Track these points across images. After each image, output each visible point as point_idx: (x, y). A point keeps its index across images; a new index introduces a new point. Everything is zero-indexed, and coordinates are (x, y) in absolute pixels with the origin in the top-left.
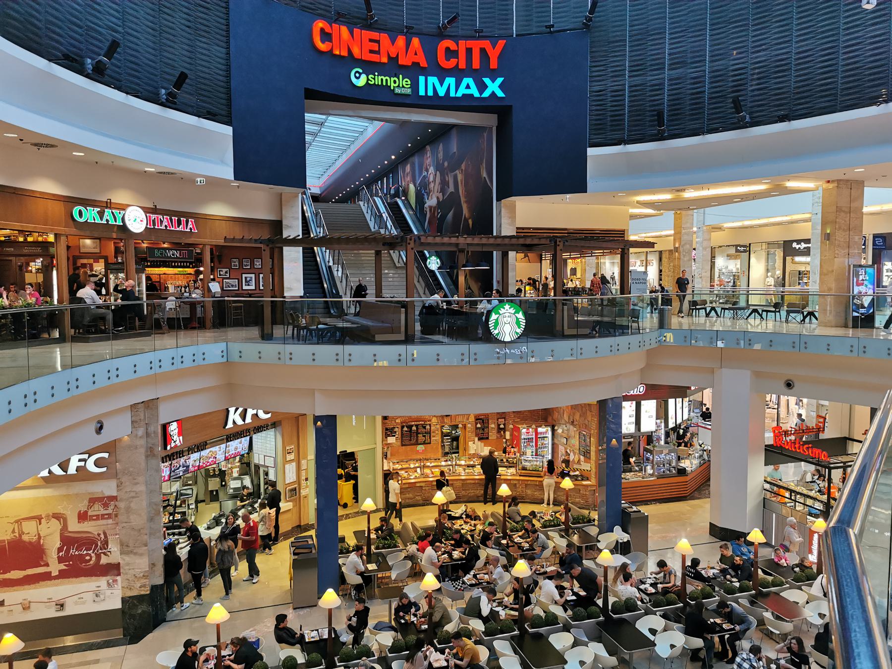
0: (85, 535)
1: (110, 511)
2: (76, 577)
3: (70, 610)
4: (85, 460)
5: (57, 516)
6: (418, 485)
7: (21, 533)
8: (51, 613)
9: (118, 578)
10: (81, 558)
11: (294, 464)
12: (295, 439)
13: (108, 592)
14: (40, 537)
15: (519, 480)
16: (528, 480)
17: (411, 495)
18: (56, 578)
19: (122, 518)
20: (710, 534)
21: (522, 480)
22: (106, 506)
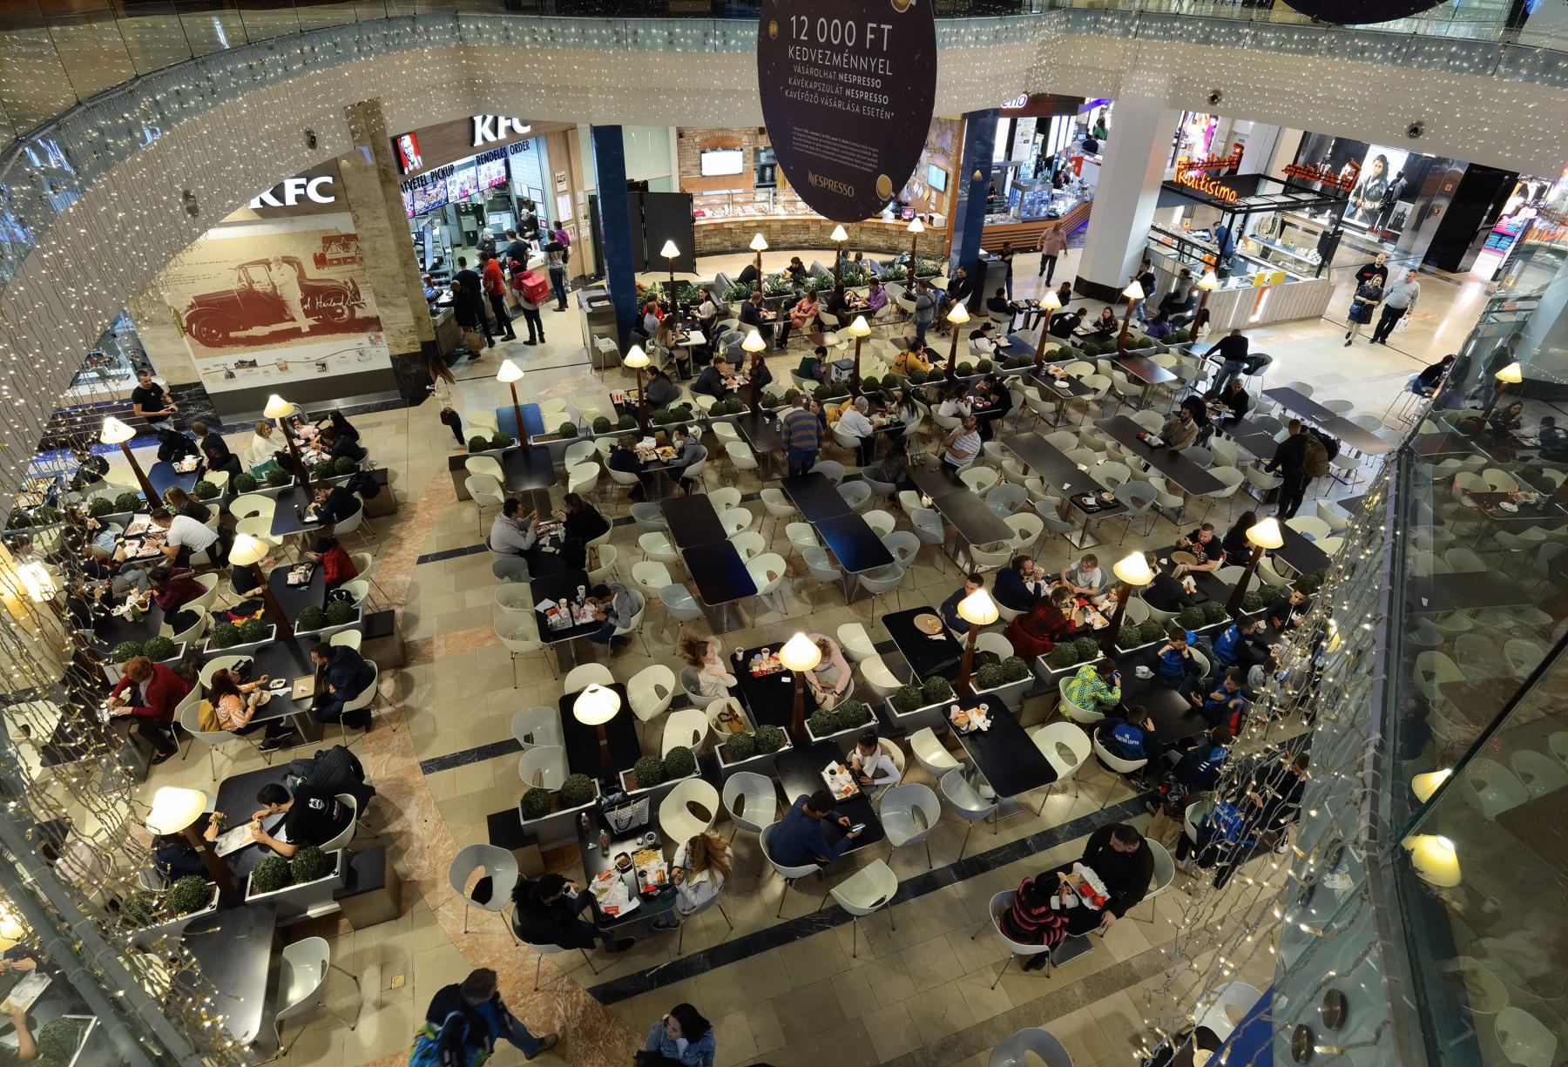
0: (328, 284)
1: (352, 254)
3: (335, 370)
5: (289, 261)
6: (726, 226)
7: (251, 282)
8: (313, 374)
9: (381, 334)
10: (332, 311)
11: (568, 197)
13: (373, 350)
14: (274, 287)
17: (717, 240)
22: (345, 247)
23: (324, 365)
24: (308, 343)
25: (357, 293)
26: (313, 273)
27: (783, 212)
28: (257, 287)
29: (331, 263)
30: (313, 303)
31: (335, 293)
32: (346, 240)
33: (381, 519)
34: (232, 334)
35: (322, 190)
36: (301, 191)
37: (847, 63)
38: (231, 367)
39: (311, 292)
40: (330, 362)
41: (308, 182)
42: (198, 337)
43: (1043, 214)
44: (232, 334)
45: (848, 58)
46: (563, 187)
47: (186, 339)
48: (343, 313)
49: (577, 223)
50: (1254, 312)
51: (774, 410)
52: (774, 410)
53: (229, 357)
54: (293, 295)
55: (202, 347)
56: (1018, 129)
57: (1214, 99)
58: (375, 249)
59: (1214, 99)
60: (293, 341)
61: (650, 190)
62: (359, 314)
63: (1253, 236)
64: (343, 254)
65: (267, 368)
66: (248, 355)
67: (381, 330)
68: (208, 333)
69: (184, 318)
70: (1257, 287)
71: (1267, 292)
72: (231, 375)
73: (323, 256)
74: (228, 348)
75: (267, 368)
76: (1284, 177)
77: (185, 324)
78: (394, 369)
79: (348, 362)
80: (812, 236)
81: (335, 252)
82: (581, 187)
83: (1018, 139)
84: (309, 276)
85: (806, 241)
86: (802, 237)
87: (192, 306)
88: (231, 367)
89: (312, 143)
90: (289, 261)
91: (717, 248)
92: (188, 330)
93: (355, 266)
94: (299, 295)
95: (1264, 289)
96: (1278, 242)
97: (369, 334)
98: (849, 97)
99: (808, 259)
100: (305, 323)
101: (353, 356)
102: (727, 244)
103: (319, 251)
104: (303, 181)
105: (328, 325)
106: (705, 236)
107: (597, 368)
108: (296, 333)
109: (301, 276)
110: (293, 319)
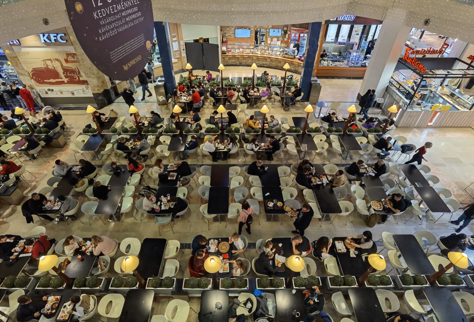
0: (70, 68)
1: (76, 59)
2: (71, 84)
3: (76, 95)
4: (56, 37)
5: (57, 60)
6: (237, 56)
7: (47, 66)
8: (70, 95)
9: (89, 86)
10: (73, 77)
11: (177, 42)
12: (176, 31)
13: (87, 91)
14: (54, 68)
15: (282, 59)
16: (286, 60)
17: (234, 61)
18: (66, 83)
19: (81, 63)
20: (357, 98)
21: (283, 60)
22: (73, 57)
23: (73, 93)
24: (67, 86)
25: (79, 73)
26: (65, 64)
27: (259, 53)
28: (49, 67)
29: (70, 62)
30: (67, 74)
31: (73, 71)
32: (74, 55)
33: (57, 149)
34: (45, 81)
35: (61, 38)
36: (55, 38)
37: (124, 7)
38: (47, 90)
39: (66, 71)
40: (75, 92)
41: (57, 35)
42: (35, 80)
43: (359, 65)
44: (45, 81)
45: (123, 4)
46: (175, 39)
47: (32, 80)
48: (76, 78)
49: (180, 52)
50: (431, 121)
51: (187, 134)
52: (187, 134)
53: (46, 87)
54: (61, 71)
55: (37, 84)
56: (354, 29)
57: (427, 22)
58: (82, 59)
59: (427, 22)
60: (63, 85)
61: (210, 43)
62: (81, 79)
63: (447, 86)
64: (73, 60)
65: (57, 92)
66: (51, 87)
67: (88, 85)
68: (38, 80)
69: (31, 74)
70: (432, 111)
71: (439, 113)
72: (47, 93)
73: (67, 59)
74: (45, 85)
75: (57, 92)
76: (469, 61)
77: (31, 76)
78: (94, 97)
79: (80, 93)
80: (267, 63)
81: (70, 58)
82: (182, 39)
83: (354, 33)
84: (64, 65)
85: (266, 64)
86: (264, 63)
87: (32, 71)
88: (47, 90)
89: (46, 22)
90: (57, 60)
91: (234, 64)
92: (32, 78)
93: (77, 64)
94: (62, 71)
95: (436, 113)
96: (457, 90)
97: (85, 85)
98: (128, 21)
99: (271, 72)
100: (66, 80)
101: (81, 91)
102: (237, 62)
103: (66, 58)
104: (56, 35)
105: (72, 81)
106: (229, 59)
107: (159, 105)
108: (63, 83)
109: (62, 65)
110: (61, 78)
